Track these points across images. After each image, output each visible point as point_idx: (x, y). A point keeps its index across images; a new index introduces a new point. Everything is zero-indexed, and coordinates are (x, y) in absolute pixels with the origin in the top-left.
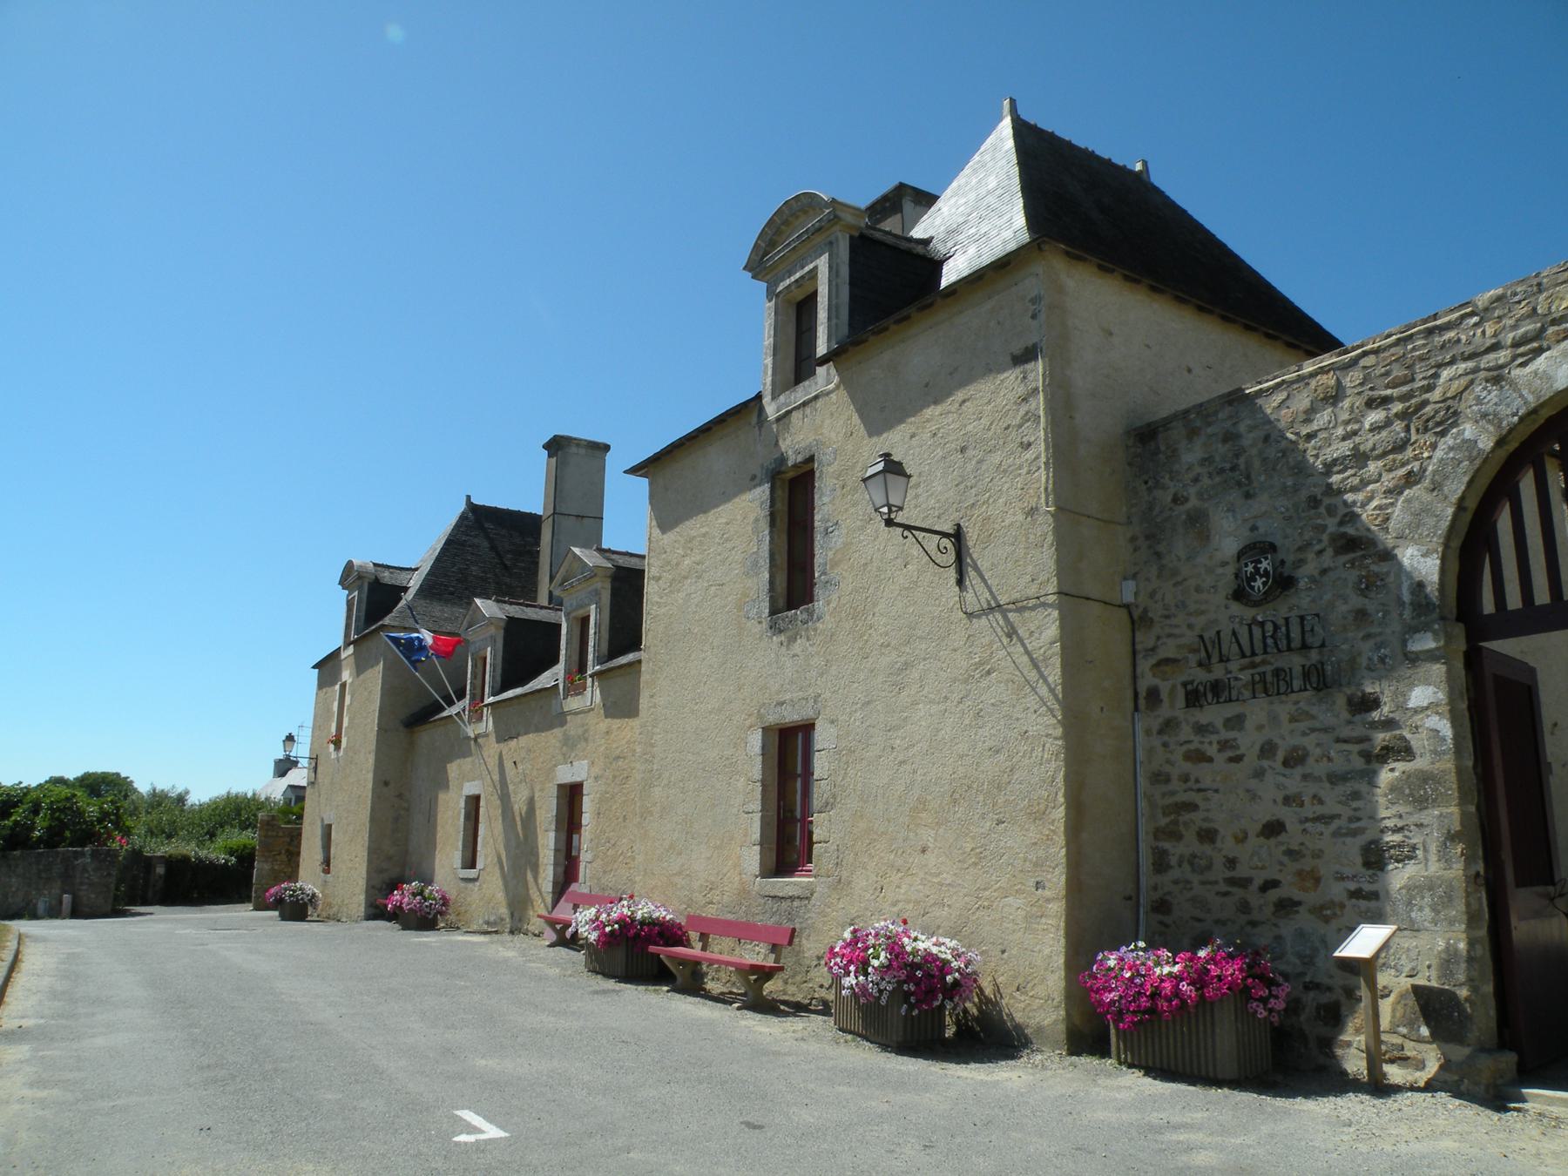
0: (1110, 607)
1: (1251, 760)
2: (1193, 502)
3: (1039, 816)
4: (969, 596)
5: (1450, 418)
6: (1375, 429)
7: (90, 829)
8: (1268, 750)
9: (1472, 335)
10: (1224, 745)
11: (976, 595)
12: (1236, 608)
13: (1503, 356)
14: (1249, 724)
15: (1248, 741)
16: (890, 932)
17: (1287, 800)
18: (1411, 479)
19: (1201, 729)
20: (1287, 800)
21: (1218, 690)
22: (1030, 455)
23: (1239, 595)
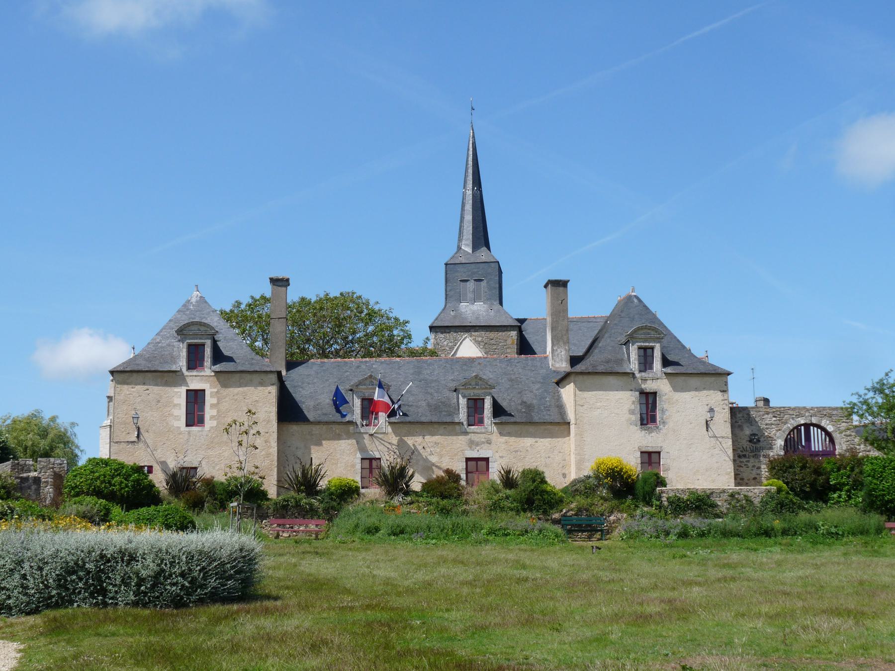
0: (142, 374)
1: (750, 468)
2: (740, 423)
3: (728, 474)
4: (709, 433)
5: (786, 423)
6: (775, 421)
7: (138, 481)
8: (754, 466)
9: (791, 412)
10: (745, 465)
11: (711, 433)
12: (748, 443)
13: (794, 416)
14: (751, 462)
15: (750, 465)
16: (889, 665)
17: (757, 474)
18: (780, 430)
19: (741, 462)
20: (757, 474)
21: (745, 456)
22: (725, 411)
23: (751, 441)
